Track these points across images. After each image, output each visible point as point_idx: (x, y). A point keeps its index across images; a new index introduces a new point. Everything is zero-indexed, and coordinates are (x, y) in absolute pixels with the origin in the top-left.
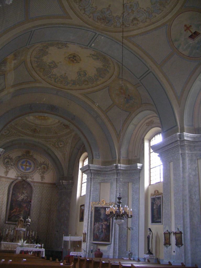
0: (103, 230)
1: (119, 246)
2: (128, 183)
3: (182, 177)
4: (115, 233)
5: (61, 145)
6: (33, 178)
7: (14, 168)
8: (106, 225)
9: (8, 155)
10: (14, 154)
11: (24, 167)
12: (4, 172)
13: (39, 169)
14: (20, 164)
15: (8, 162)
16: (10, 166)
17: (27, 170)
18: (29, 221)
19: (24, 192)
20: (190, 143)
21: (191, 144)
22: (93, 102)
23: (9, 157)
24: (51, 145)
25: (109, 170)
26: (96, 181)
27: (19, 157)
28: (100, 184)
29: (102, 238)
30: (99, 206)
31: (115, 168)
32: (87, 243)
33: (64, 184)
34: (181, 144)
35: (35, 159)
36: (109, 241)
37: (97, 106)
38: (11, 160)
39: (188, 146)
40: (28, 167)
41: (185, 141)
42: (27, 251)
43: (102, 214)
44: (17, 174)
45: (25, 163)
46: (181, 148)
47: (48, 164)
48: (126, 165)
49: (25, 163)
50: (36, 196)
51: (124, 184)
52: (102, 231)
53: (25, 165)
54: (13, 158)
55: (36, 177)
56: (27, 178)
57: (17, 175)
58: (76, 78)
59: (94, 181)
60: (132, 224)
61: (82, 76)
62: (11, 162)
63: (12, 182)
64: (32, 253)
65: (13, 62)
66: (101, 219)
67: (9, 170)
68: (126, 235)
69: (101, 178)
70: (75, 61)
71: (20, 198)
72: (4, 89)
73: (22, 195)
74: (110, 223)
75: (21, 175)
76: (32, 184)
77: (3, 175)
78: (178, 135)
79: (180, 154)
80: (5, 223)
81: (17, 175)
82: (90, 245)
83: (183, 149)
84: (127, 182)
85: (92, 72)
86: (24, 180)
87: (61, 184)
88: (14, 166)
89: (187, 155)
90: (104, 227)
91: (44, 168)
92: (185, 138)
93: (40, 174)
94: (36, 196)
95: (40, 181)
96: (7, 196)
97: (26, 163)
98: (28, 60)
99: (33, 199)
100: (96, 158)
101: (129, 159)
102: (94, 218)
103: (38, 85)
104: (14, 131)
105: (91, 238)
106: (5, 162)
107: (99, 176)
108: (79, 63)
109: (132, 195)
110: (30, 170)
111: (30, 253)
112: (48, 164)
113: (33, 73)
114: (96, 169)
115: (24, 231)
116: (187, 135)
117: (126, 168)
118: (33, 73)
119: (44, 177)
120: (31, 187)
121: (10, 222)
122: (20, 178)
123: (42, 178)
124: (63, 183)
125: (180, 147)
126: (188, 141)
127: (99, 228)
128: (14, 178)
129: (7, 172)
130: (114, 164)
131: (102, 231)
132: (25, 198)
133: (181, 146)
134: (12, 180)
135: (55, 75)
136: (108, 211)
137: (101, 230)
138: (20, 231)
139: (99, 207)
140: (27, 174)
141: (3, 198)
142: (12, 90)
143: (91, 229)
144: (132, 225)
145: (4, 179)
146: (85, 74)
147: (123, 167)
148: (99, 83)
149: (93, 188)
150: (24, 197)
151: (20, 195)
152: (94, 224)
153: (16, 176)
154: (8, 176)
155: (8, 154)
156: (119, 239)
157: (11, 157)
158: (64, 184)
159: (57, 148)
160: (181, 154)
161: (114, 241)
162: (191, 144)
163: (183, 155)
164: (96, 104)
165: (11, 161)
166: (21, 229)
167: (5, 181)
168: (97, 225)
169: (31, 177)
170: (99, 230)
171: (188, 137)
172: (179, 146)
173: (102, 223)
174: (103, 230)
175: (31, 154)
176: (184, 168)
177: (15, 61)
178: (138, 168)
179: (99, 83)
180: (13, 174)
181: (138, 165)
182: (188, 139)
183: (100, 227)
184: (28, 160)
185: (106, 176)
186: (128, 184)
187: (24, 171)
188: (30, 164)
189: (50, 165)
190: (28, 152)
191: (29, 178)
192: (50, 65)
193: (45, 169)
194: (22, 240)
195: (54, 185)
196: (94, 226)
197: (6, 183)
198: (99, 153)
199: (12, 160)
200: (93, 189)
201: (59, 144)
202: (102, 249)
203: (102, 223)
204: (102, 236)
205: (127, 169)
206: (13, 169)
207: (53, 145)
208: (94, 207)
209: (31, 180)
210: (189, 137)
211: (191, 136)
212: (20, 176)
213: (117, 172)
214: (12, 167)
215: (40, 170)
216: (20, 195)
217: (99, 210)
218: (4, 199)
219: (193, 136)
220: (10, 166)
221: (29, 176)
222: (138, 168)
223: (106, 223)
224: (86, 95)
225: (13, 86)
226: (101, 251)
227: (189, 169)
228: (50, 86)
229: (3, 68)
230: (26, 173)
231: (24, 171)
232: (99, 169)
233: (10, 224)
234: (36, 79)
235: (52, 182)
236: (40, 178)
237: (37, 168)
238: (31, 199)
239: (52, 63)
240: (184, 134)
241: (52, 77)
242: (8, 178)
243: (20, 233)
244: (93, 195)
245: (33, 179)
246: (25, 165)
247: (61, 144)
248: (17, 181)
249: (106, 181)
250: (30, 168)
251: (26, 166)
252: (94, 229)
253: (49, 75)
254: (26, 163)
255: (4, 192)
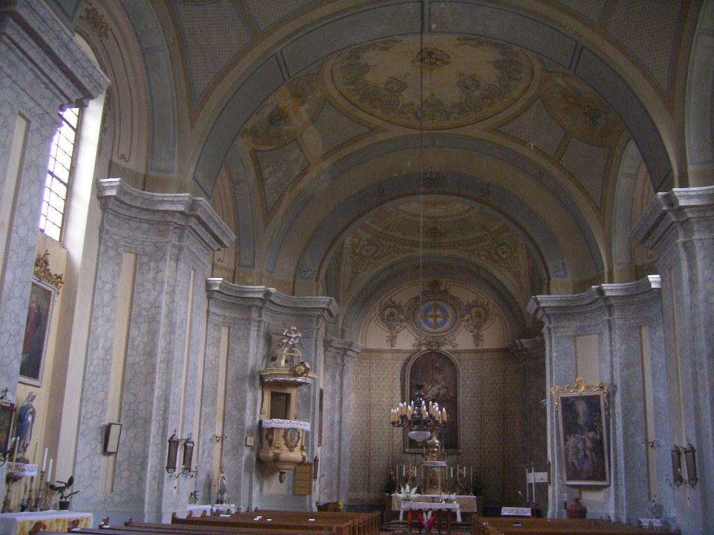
0: (588, 452)
1: (628, 491)
2: (640, 327)
3: (689, 304)
4: (616, 457)
5: (503, 253)
6: (454, 342)
7: (408, 326)
8: (593, 440)
9: (390, 299)
10: (403, 296)
11: (431, 320)
12: (386, 338)
13: (465, 318)
14: (419, 316)
15: (391, 314)
16: (398, 323)
17: (437, 325)
18: (434, 443)
19: (439, 378)
20: (704, 211)
21: (708, 214)
22: (524, 143)
23: (393, 303)
24: (483, 258)
25: (587, 302)
26: (563, 334)
27: (417, 299)
28: (575, 340)
29: (588, 472)
30: (571, 393)
31: (597, 296)
32: (554, 485)
33: (525, 347)
34: (681, 219)
35: (454, 298)
36: (604, 479)
37: (532, 148)
38: (397, 309)
39: (697, 219)
40: (439, 320)
41: (687, 210)
42: (421, 510)
43: (581, 414)
44: (416, 339)
45: (432, 310)
46: (684, 229)
47: (486, 303)
48: (629, 284)
49: (432, 310)
50: (468, 383)
51: (627, 332)
52: (586, 456)
53: (432, 316)
54: (403, 303)
55: (463, 340)
56: (439, 345)
57: (416, 342)
58: (461, 96)
59: (558, 334)
60: (656, 432)
61: (472, 89)
62: (399, 314)
63: (409, 359)
64: (430, 513)
65: (302, 109)
66: (579, 425)
67: (398, 332)
68: (645, 461)
69: (575, 325)
70: (438, 63)
71: (429, 393)
72: (306, 168)
73: (433, 386)
74: (601, 433)
75: (425, 339)
76: (454, 358)
77: (386, 346)
78: (660, 198)
79: (680, 245)
80: (404, 452)
81: (416, 342)
82: (561, 491)
83: (689, 232)
84: (635, 325)
85: (489, 75)
86: (433, 352)
87: (520, 348)
88: (406, 321)
89: (697, 244)
90: (589, 444)
91: (479, 315)
92: (682, 203)
93: (471, 332)
94: (468, 383)
95: (472, 346)
96: (400, 392)
97: (435, 311)
98: (334, 94)
99: (461, 392)
100: (557, 276)
101: (636, 266)
102: (564, 425)
103: (381, 137)
104: (389, 243)
105: (562, 474)
106: (386, 317)
107: (569, 320)
108: (448, 63)
109: (652, 359)
110: (447, 325)
111: (427, 514)
112: (488, 305)
113: (362, 116)
114: (555, 305)
115: (442, 467)
116: (686, 194)
117: (626, 290)
118: (362, 116)
119: (482, 336)
120: (452, 364)
121: (413, 450)
122: (424, 348)
123: (477, 338)
124: (522, 345)
125: (678, 226)
126: (694, 206)
127: (578, 447)
128: (412, 348)
129: (392, 339)
130: (593, 287)
131: (586, 456)
132: (441, 391)
133: (682, 223)
134: (407, 355)
135: (411, 104)
136: (12, 437)
137: (582, 453)
138: (432, 467)
139: (572, 397)
140: (439, 335)
141: (392, 398)
142: (326, 165)
143: (559, 452)
144: (657, 436)
145: (389, 356)
146: (477, 85)
147: (618, 289)
148: (516, 93)
149: (557, 352)
150: (439, 389)
151: (430, 387)
152: (566, 440)
153: (414, 345)
154: (398, 346)
155: (389, 297)
156: (626, 473)
157: (397, 303)
158: (525, 347)
159: (498, 262)
160: (684, 244)
161: (616, 479)
162: (708, 214)
163: (688, 246)
164: (528, 144)
165: (399, 311)
166: (434, 464)
167: (392, 360)
168: (572, 440)
169: (449, 342)
170: (577, 452)
171: (690, 197)
172: (675, 224)
173: (583, 437)
174: (588, 452)
175: (442, 288)
176: (693, 281)
177: (307, 106)
178: (653, 286)
179: (516, 93)
180: (407, 341)
181: (650, 280)
182: (692, 203)
183: (580, 446)
184: (439, 303)
185: (586, 318)
186: (640, 331)
187: (431, 330)
188: (444, 310)
189: (491, 307)
190: (435, 284)
191: (446, 344)
192: (389, 86)
193: (479, 316)
194: (408, 487)
195: (508, 353)
196: (565, 444)
197: (395, 364)
198: (563, 264)
199: (400, 310)
200: (555, 354)
201: (500, 252)
202: (588, 497)
203: (583, 437)
204: (587, 466)
205: (629, 293)
206: (406, 330)
207: (485, 256)
208: (560, 399)
209: (450, 348)
210: (694, 196)
211: (699, 193)
212: (424, 342)
213: (607, 304)
214: (402, 324)
215: (470, 322)
216: (430, 387)
217: (572, 404)
218: (394, 400)
219: (706, 193)
220: (398, 323)
221: (446, 339)
222: (653, 286)
223: (591, 434)
224: (499, 129)
225: (324, 158)
226: (584, 505)
227: (705, 282)
228: (410, 132)
229: (286, 128)
230: (436, 333)
231: (431, 330)
232: (563, 304)
233: (415, 453)
234: (372, 126)
235: (502, 347)
236: (472, 339)
237: (463, 316)
238: (456, 393)
239: (391, 82)
240: (673, 192)
241: (405, 110)
242: (398, 351)
243: (434, 474)
244: (559, 370)
245: (457, 345)
246: (432, 316)
247: (505, 250)
248: (417, 355)
249: (589, 329)
250: (445, 321)
251: (436, 316)
252: (565, 452)
253: (399, 108)
254: (435, 311)
255: (392, 382)
